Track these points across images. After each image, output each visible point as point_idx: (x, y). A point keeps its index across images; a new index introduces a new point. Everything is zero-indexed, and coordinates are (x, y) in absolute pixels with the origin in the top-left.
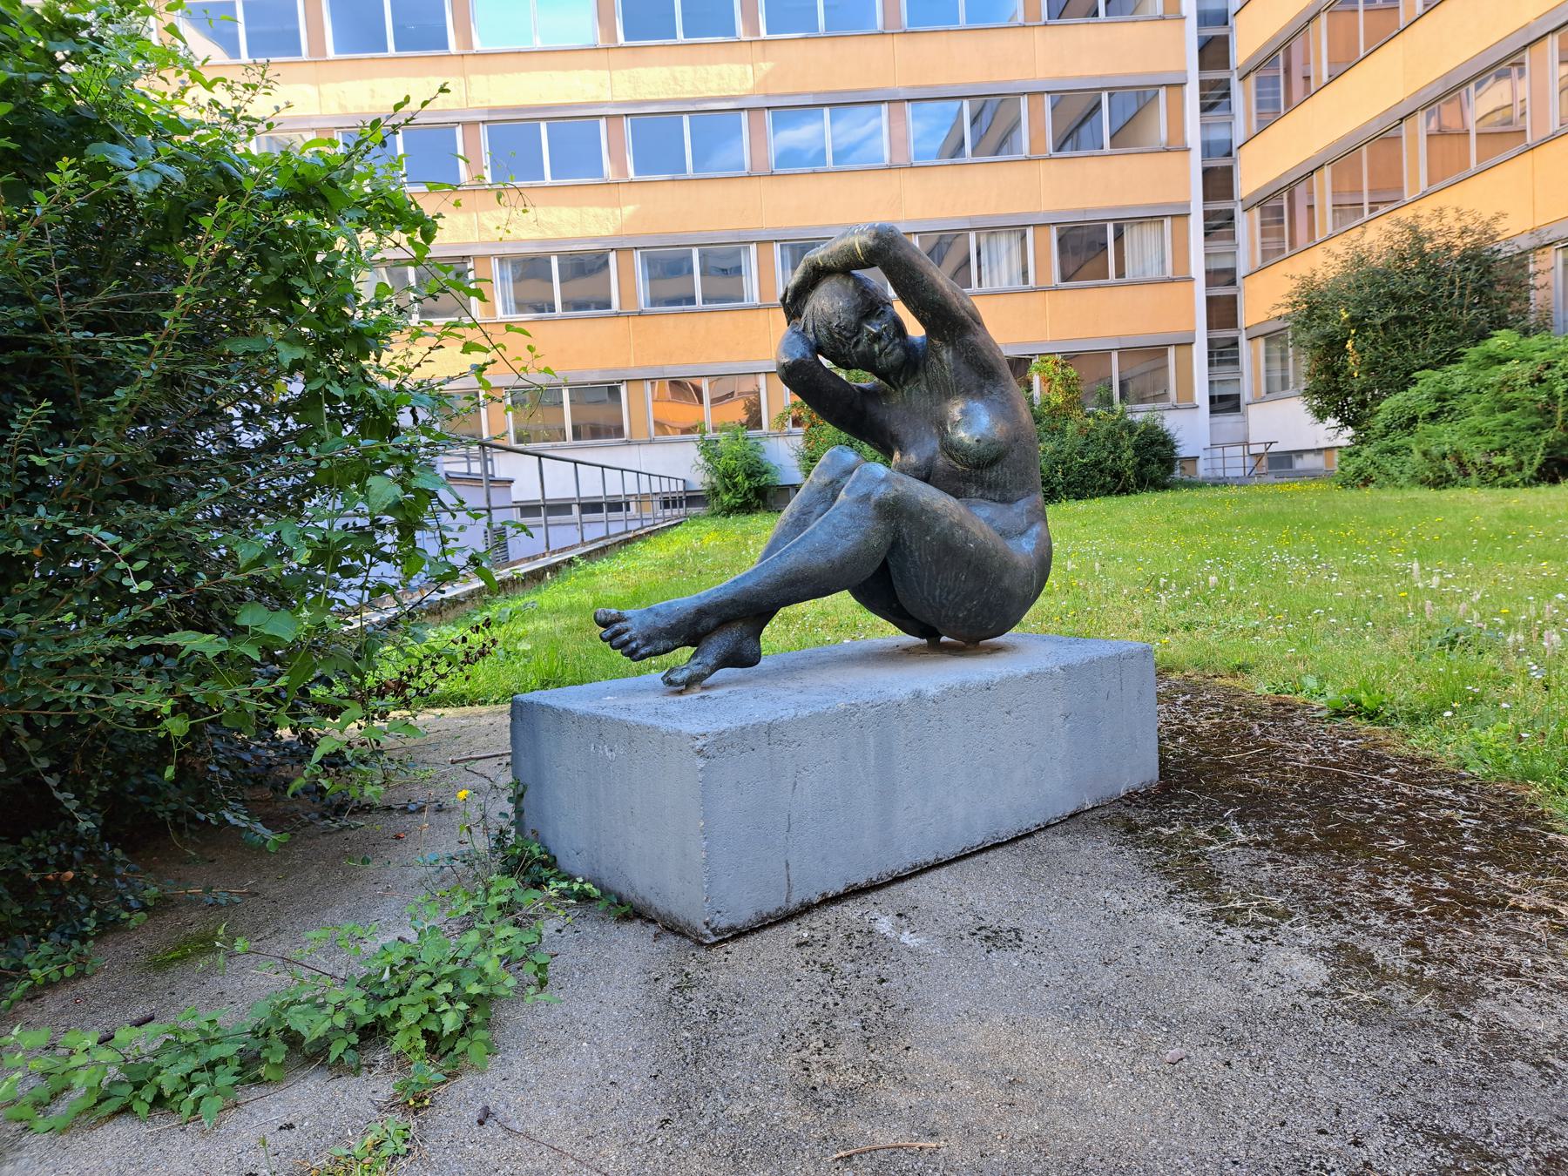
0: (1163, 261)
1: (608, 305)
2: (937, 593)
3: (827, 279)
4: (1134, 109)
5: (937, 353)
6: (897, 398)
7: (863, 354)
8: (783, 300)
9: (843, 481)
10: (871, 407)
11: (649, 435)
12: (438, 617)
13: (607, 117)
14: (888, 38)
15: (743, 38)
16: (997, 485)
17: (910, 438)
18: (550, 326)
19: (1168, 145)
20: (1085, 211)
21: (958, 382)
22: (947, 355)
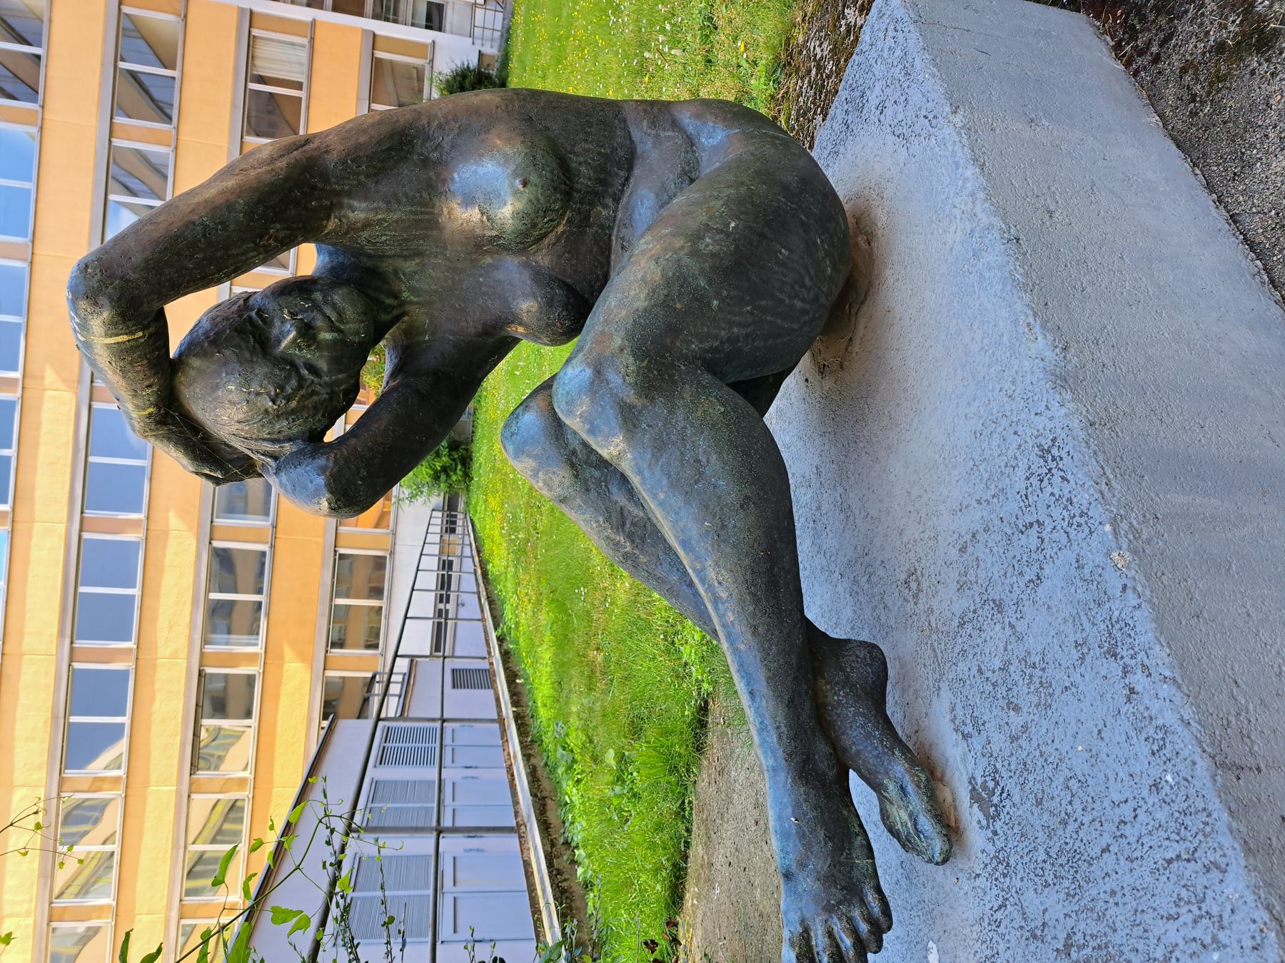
0: (292, 44)
1: (263, 554)
2: (798, 304)
3: (185, 402)
4: (141, 43)
5: (352, 228)
6: (419, 316)
7: (336, 362)
8: (217, 481)
9: (575, 444)
10: (430, 360)
11: (388, 534)
12: (549, 802)
13: (81, 530)
14: (36, 258)
15: (19, 394)
16: (603, 169)
17: (494, 306)
18: (274, 608)
19: (179, 15)
20: (234, 106)
21: (412, 201)
22: (358, 211)
